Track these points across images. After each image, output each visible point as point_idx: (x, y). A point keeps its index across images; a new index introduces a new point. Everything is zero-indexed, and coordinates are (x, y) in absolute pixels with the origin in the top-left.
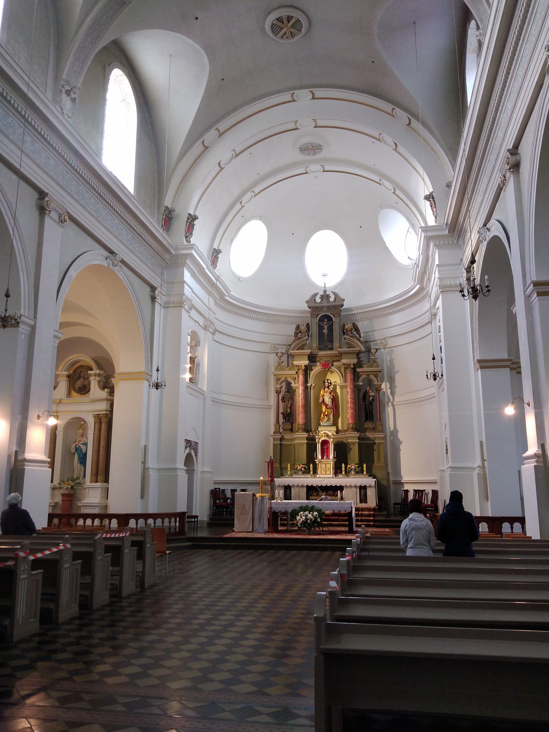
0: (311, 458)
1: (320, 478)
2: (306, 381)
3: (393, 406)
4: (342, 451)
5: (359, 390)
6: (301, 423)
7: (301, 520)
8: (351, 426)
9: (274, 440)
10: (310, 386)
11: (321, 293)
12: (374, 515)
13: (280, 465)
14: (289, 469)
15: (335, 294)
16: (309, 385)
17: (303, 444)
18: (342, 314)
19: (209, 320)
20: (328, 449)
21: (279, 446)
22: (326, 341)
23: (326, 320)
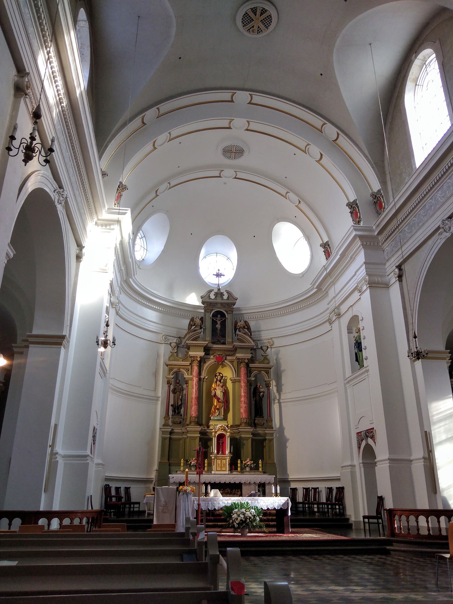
0: (204, 454)
1: (215, 474)
2: (200, 373)
3: (280, 403)
4: (236, 444)
5: (251, 385)
6: (193, 416)
7: (239, 519)
8: (245, 421)
9: (163, 433)
10: (204, 379)
11: (216, 290)
13: (168, 460)
14: (182, 464)
15: (228, 292)
16: (202, 377)
17: (196, 438)
18: (234, 313)
20: (224, 443)
21: (168, 440)
22: (219, 335)
23: (219, 316)
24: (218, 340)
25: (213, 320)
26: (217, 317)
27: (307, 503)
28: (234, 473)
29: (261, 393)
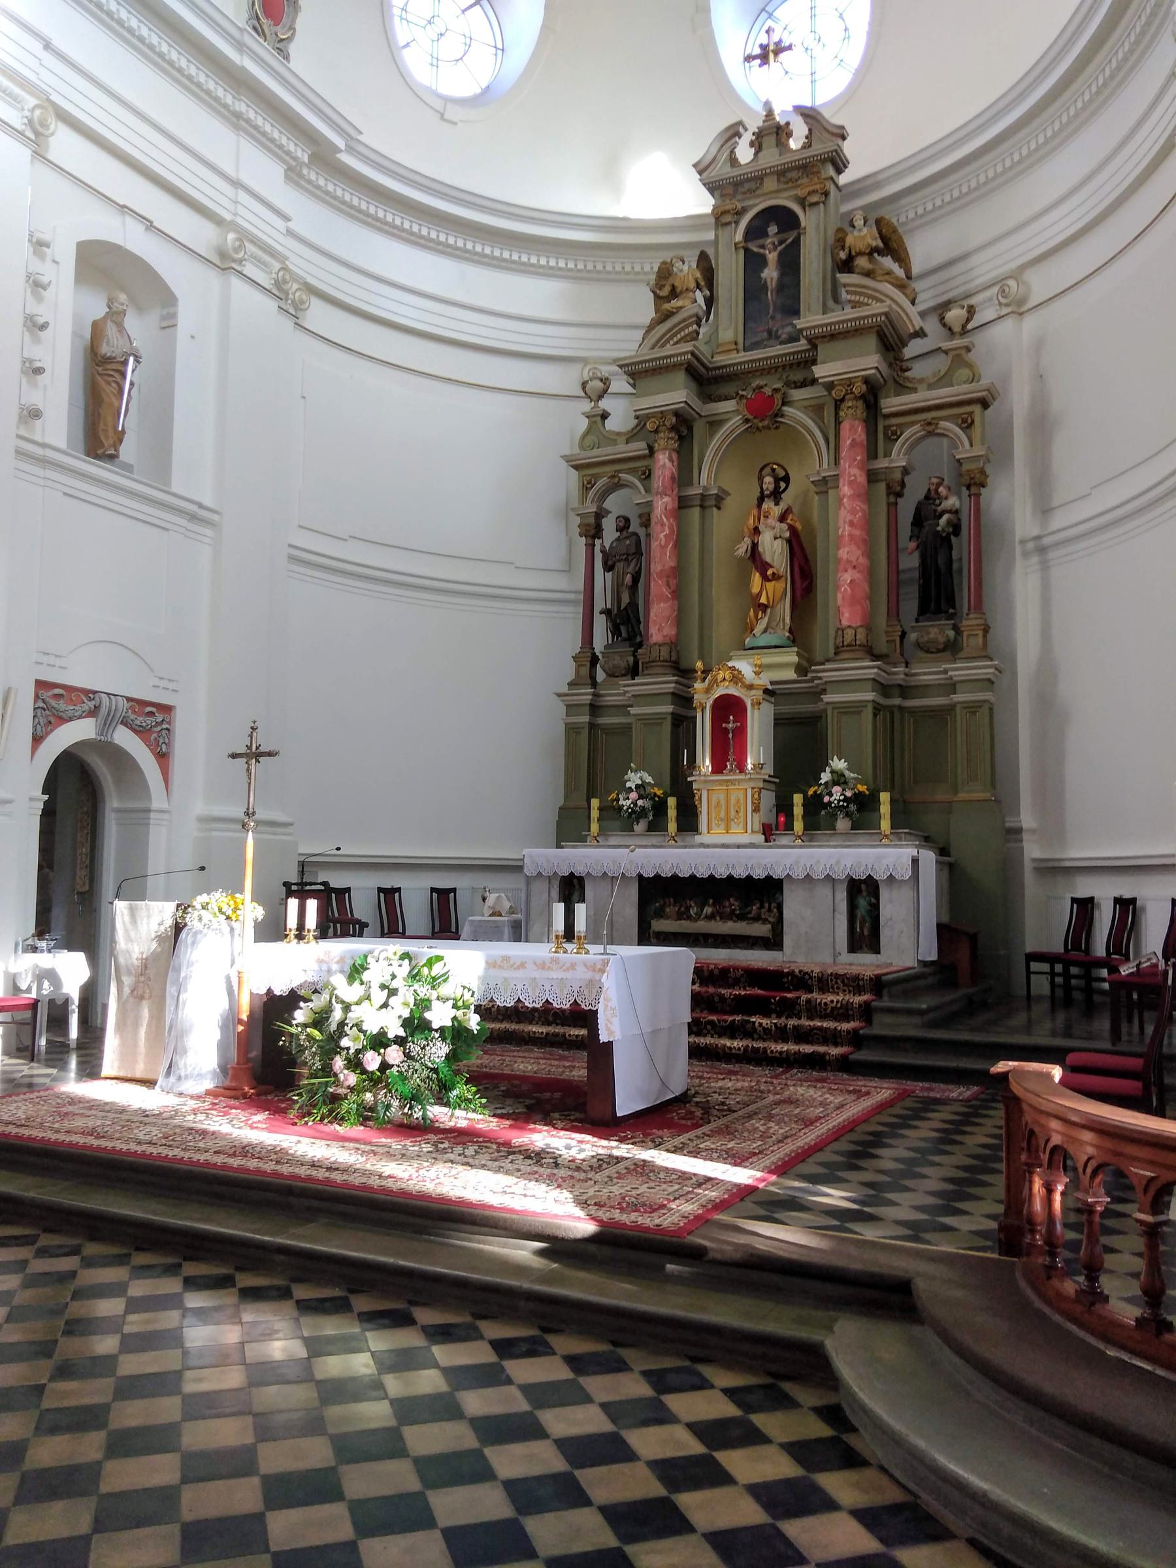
1: (702, 845)
4: (801, 743)
12: (866, 1012)
19: (232, 226)
20: (741, 731)
23: (773, 229)
24: (770, 332)
25: (746, 250)
26: (766, 235)
27: (1076, 963)
28: (784, 840)
29: (941, 516)
